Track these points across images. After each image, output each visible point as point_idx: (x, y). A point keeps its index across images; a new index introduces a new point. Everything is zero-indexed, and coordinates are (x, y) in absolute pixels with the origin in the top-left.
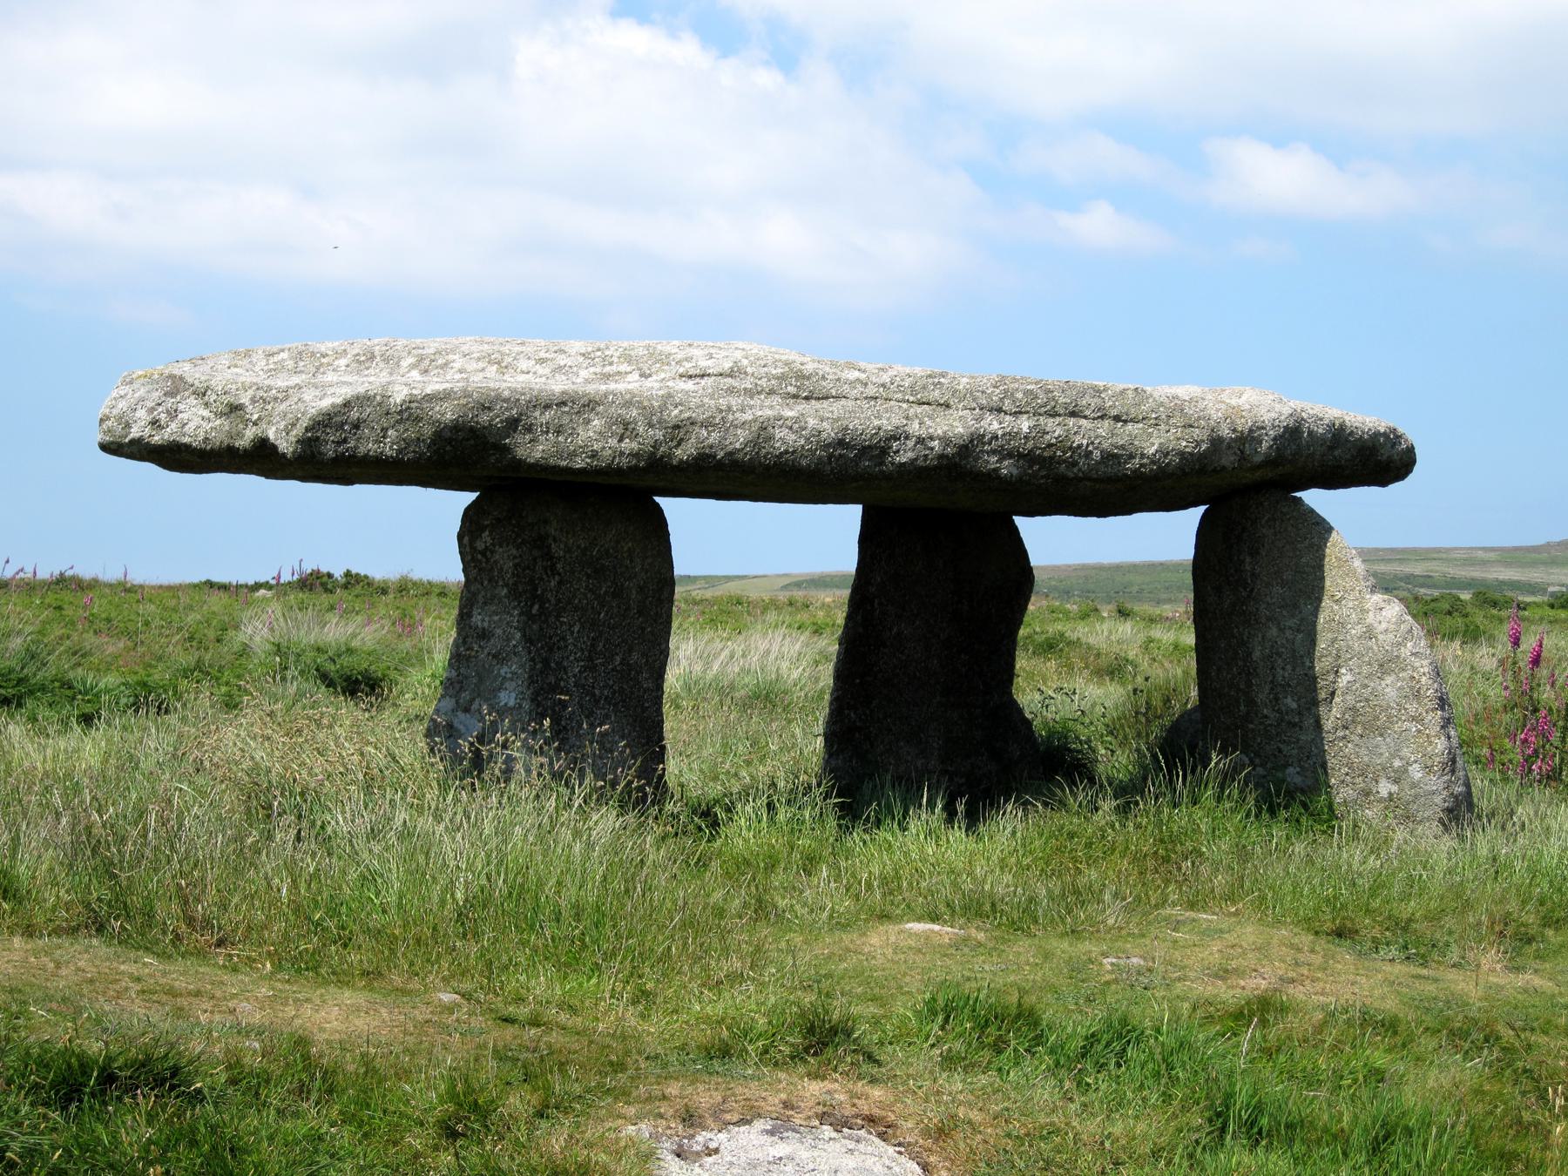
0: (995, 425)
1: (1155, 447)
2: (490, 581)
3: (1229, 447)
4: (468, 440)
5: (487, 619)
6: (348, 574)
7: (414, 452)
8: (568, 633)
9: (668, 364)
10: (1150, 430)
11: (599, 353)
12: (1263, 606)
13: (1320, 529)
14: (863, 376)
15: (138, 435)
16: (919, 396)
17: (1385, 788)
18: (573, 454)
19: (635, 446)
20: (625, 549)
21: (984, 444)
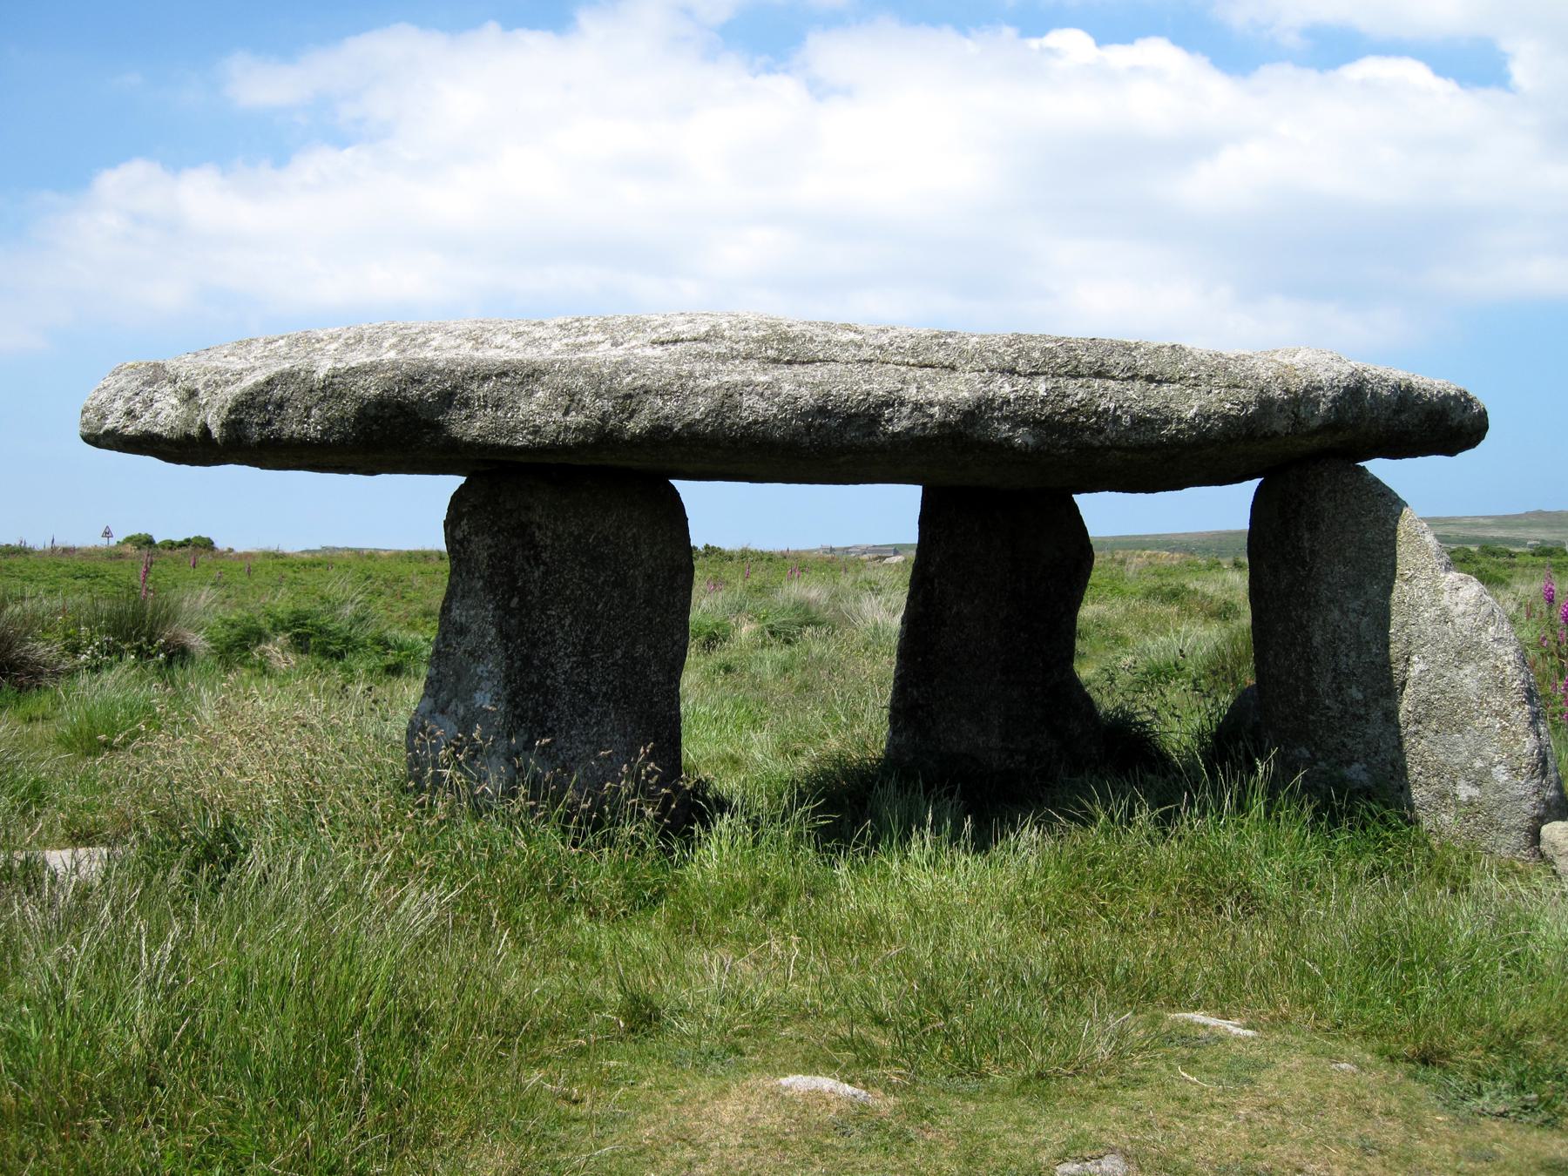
0: (1007, 388)
1: (1195, 410)
2: (468, 573)
3: (1281, 410)
4: (396, 417)
5: (464, 614)
6: (707, 547)
7: (338, 432)
8: (557, 627)
9: (644, 331)
10: (1189, 391)
11: (577, 324)
12: (1325, 586)
13: (1388, 504)
14: (858, 338)
15: (111, 426)
16: (920, 359)
17: (1465, 791)
18: (513, 431)
19: (581, 419)
20: (629, 535)
21: (993, 410)
